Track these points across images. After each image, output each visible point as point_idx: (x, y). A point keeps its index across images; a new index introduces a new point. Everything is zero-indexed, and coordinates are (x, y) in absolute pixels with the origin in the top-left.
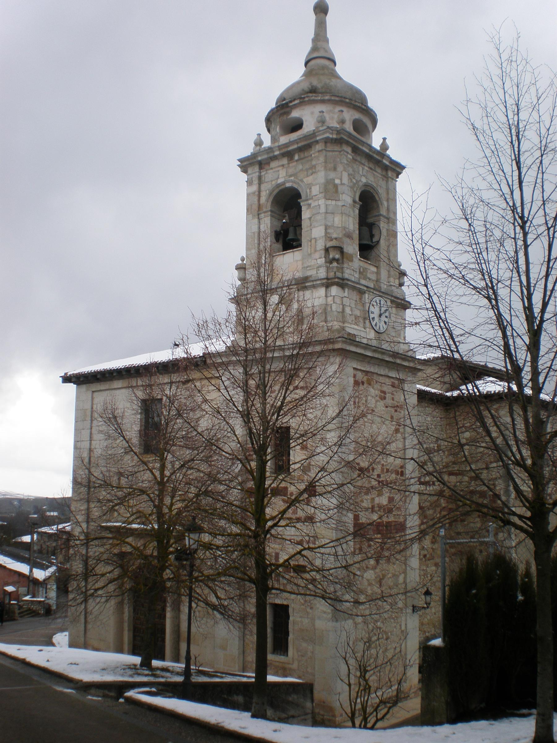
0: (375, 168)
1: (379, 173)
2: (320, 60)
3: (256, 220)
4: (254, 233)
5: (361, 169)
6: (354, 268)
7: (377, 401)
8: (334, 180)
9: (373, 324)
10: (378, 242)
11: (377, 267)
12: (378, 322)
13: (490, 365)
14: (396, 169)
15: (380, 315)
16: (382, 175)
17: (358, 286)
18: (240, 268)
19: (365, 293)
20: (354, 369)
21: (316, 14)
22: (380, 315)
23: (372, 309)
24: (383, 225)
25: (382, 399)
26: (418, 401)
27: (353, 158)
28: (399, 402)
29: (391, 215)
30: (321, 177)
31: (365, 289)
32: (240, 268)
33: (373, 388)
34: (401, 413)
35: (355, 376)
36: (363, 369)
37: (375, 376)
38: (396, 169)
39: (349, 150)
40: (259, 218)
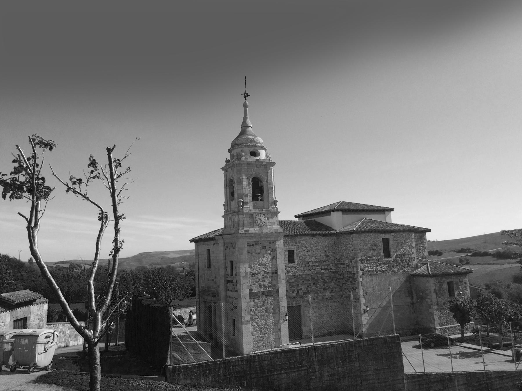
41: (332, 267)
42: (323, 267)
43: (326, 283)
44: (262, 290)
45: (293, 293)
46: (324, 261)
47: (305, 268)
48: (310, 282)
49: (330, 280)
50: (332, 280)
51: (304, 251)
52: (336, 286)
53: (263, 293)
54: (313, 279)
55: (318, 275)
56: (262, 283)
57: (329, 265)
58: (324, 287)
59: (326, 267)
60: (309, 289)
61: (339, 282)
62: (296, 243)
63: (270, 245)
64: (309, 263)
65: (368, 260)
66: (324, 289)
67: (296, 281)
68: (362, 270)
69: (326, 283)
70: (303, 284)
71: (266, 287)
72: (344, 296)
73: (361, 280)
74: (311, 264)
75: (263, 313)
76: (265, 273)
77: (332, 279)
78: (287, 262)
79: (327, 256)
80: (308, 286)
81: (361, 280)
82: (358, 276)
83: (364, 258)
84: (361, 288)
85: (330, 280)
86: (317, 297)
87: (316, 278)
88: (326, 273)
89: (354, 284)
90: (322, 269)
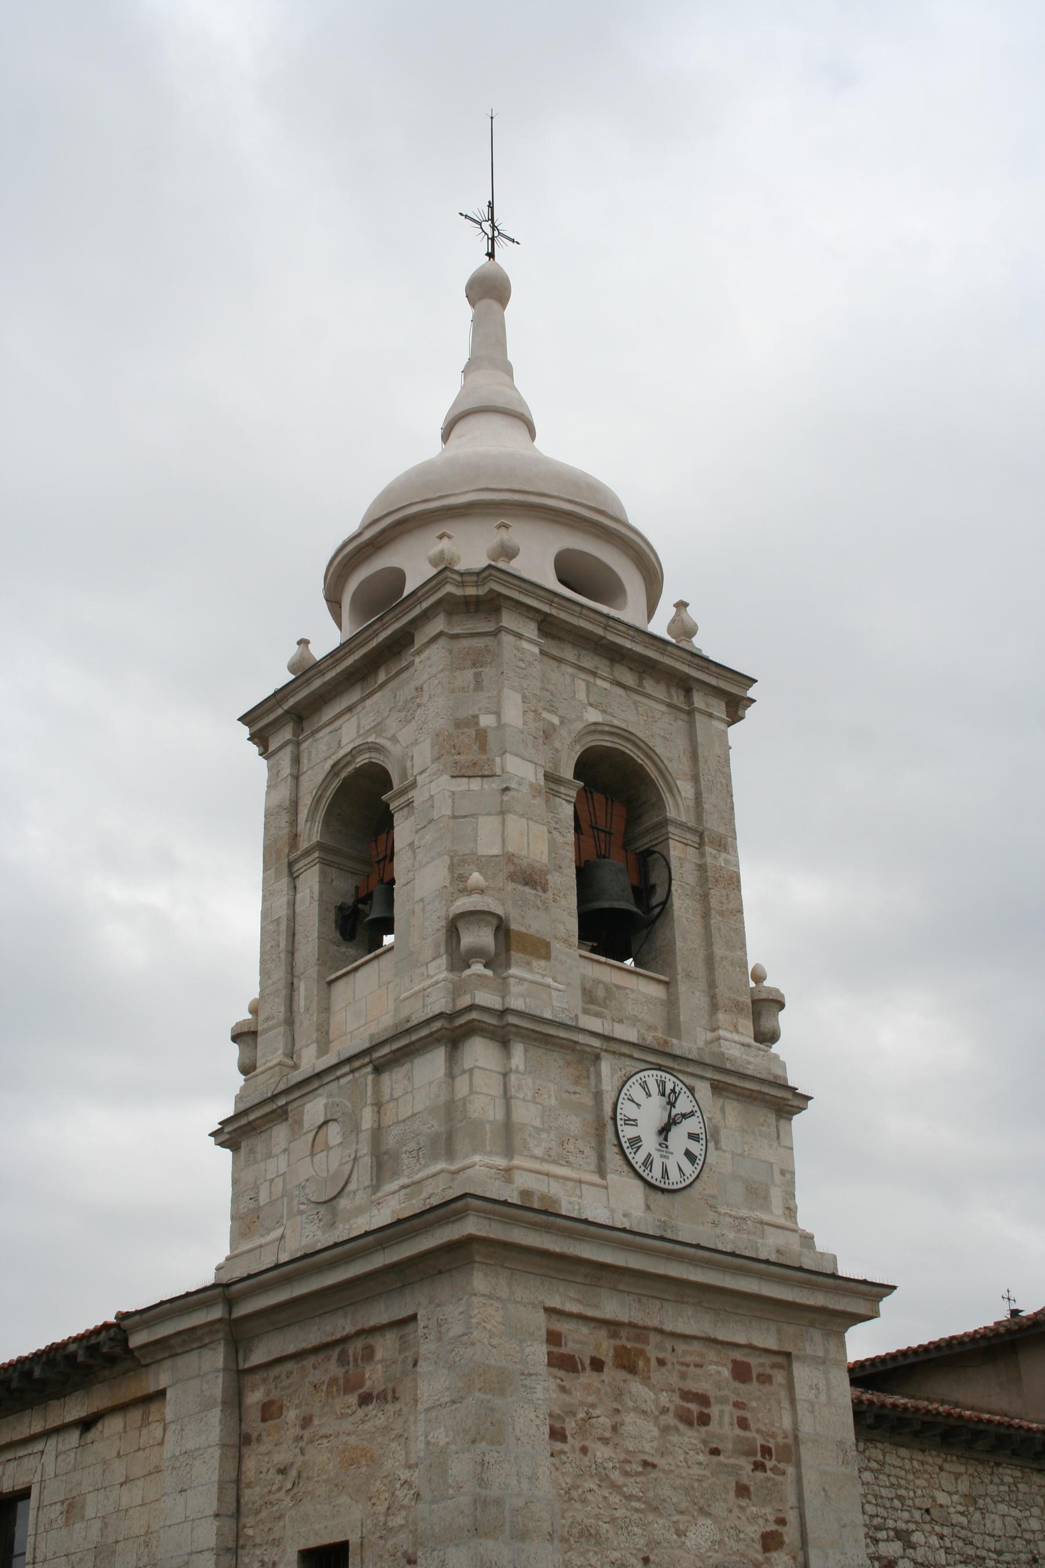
0: (640, 685)
3: (285, 881)
4: (278, 921)
5: (581, 686)
6: (559, 979)
7: (665, 1430)
8: (476, 717)
9: (638, 1159)
10: (666, 903)
11: (666, 983)
12: (656, 1155)
14: (733, 694)
15: (664, 1131)
16: (669, 705)
17: (581, 1038)
18: (243, 1036)
19: (597, 1058)
20: (550, 1311)
21: (473, 303)
22: (664, 1131)
23: (626, 1109)
24: (680, 855)
25: (690, 1424)
26: (858, 1434)
27: (542, 652)
28: (773, 1435)
29: (712, 823)
30: (436, 711)
31: (596, 1043)
32: (243, 1036)
33: (646, 1380)
34: (784, 1473)
35: (553, 1338)
36: (590, 1313)
37: (654, 1338)
38: (733, 694)
39: (530, 630)
40: (291, 873)
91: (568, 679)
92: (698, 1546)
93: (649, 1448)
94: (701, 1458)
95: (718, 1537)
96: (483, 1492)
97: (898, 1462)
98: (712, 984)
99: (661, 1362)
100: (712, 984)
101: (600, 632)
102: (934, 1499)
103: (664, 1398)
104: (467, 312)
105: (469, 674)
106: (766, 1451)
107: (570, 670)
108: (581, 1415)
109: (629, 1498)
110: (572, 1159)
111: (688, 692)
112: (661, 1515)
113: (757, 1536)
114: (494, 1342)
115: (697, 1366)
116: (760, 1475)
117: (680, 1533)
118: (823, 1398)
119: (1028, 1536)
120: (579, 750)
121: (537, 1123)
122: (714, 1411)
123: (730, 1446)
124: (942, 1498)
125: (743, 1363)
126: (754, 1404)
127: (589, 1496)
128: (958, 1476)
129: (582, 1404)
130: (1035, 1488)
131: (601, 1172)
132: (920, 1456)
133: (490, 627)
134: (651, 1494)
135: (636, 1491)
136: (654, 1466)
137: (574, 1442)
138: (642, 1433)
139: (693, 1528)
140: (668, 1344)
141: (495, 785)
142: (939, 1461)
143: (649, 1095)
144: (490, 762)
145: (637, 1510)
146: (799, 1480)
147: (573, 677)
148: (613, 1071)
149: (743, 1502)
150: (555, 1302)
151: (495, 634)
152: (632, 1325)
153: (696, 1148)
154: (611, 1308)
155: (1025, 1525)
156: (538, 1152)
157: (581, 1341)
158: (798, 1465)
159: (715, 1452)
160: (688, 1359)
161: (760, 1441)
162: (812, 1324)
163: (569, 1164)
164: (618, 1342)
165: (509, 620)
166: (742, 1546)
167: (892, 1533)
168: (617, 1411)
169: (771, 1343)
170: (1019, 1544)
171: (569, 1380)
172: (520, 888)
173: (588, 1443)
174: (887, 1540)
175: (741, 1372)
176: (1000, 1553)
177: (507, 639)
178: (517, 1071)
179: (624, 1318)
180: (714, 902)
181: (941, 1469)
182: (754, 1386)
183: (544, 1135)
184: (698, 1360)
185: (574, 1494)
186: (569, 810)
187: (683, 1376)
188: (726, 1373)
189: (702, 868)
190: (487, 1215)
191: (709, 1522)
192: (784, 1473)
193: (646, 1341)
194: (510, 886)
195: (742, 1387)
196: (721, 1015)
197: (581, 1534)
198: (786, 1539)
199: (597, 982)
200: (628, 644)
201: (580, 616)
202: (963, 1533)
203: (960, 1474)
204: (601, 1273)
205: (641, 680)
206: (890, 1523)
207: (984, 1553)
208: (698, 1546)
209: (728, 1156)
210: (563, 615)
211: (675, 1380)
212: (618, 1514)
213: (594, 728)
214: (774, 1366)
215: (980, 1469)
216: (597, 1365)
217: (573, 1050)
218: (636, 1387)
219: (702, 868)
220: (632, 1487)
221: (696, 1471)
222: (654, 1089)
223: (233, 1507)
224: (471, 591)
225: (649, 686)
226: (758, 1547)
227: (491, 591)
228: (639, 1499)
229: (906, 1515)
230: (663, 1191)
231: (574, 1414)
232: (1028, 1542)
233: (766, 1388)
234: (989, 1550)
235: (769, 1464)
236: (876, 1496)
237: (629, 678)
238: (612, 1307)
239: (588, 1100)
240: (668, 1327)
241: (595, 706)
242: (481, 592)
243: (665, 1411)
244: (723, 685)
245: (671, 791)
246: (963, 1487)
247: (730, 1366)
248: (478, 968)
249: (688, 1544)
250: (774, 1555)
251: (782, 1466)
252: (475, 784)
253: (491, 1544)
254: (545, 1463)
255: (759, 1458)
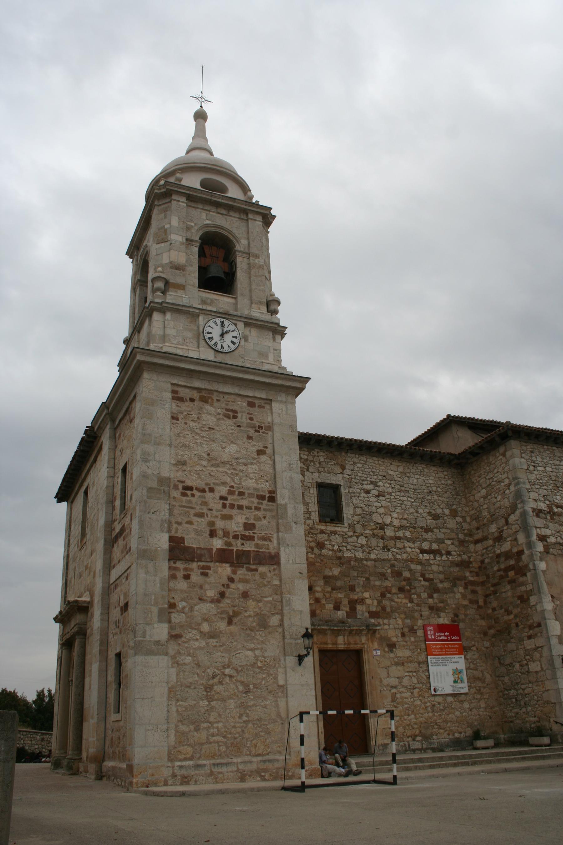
1: (213, 212)
2: (199, 142)
8: (164, 226)
13: (283, 395)
17: (191, 310)
19: (198, 316)
20: (172, 384)
22: (222, 335)
27: (187, 206)
28: (264, 423)
31: (197, 311)
33: (212, 405)
35: (174, 392)
36: (188, 385)
37: (215, 393)
39: (184, 199)
41: (451, 548)
42: (426, 546)
43: (437, 590)
44: (218, 543)
45: (337, 607)
46: (428, 530)
47: (374, 542)
48: (388, 584)
49: (446, 585)
50: (455, 585)
51: (368, 492)
52: (466, 602)
53: (224, 556)
54: (398, 574)
55: (413, 566)
56: (220, 524)
57: (440, 541)
58: (431, 601)
59: (435, 546)
60: (386, 602)
61: (474, 592)
62: (343, 468)
63: (251, 410)
64: (382, 527)
65: (554, 514)
66: (431, 608)
67: (344, 574)
68: (542, 538)
69: (437, 590)
70: (367, 586)
71: (236, 537)
72: (492, 632)
73: (542, 566)
74: (389, 532)
75: (222, 625)
76: (231, 492)
77: (455, 581)
78: (315, 516)
79: (436, 517)
80: (383, 595)
81: (542, 566)
82: (531, 556)
83: (543, 506)
84: (545, 588)
85: (446, 585)
86: (412, 631)
87: (406, 574)
88: (436, 565)
89: (523, 584)
90: (423, 551)
91: (199, 213)
92: (230, 452)
93: (211, 424)
94: (233, 428)
95: (238, 450)
96: (144, 432)
97: (373, 461)
98: (251, 297)
99: (218, 400)
100: (251, 297)
101: (210, 198)
102: (387, 473)
103: (219, 411)
104: (194, 123)
105: (163, 215)
106: (260, 427)
107: (200, 210)
108: (185, 413)
109: (203, 437)
110: (188, 344)
111: (247, 214)
112: (215, 443)
113: (255, 450)
114: (151, 391)
115: (232, 402)
116: (257, 434)
117: (223, 448)
118: (284, 412)
119: (427, 485)
120: (201, 233)
121: (175, 334)
122: (239, 415)
123: (245, 425)
124: (391, 472)
125: (252, 402)
126: (256, 414)
127: (187, 436)
128: (398, 466)
129: (185, 410)
130: (432, 471)
131: (198, 347)
132: (382, 460)
133: (168, 200)
134: (212, 436)
135: (205, 435)
136: (213, 429)
137: (181, 422)
138: (209, 419)
139: (228, 447)
140: (222, 396)
141: (168, 243)
142: (390, 462)
143: (217, 325)
144: (167, 237)
145: (206, 441)
146: (273, 436)
147: (201, 212)
148: (204, 319)
149: (250, 441)
150: (175, 381)
151: (170, 202)
152: (205, 389)
153: (235, 340)
154: (197, 384)
155: (426, 481)
156: (175, 342)
157: (183, 393)
158: (273, 432)
159: (239, 426)
160: (229, 400)
161: (257, 424)
162: (281, 391)
163: (186, 345)
164: (201, 394)
165: (174, 197)
166: (248, 453)
167: (369, 482)
168: (200, 413)
169: (263, 396)
170: (424, 487)
171: (180, 404)
172: (174, 270)
173: (188, 422)
174: (367, 484)
175: (251, 405)
176: (415, 489)
177: (173, 202)
178: (168, 320)
179: (203, 387)
180: (252, 273)
181: (391, 464)
182: (257, 409)
183: (177, 338)
184: (233, 400)
185: (180, 435)
186: (196, 249)
187: (227, 405)
188: (245, 404)
189: (249, 264)
190: (143, 354)
191: (235, 445)
192: (267, 434)
193: (213, 394)
194: (171, 270)
195: (251, 409)
196: (253, 305)
197: (183, 446)
198: (267, 452)
199: (207, 298)
200: (220, 201)
201: (201, 193)
202: (399, 483)
203: (399, 466)
204: (191, 373)
205: (228, 213)
206: (368, 479)
207: (408, 489)
208: (230, 452)
209: (252, 344)
210: (194, 194)
211: (223, 405)
212: (198, 441)
213: (207, 226)
214: (265, 403)
215: (408, 464)
216: (192, 400)
217: (189, 314)
218: (208, 407)
219: (249, 264)
220: (204, 434)
221: (231, 431)
222: (219, 323)
223: (113, 466)
224: (162, 190)
225: (232, 213)
226: (255, 454)
227: (167, 189)
228: (207, 438)
229: (375, 477)
230: (222, 352)
231: (182, 413)
232: (428, 487)
233: (262, 409)
234: (411, 489)
235: (261, 431)
236: (363, 471)
237: (223, 212)
238: (197, 384)
239: (196, 328)
240: (220, 390)
241: (205, 219)
242: (165, 190)
243: (219, 414)
244: (259, 210)
245: (238, 242)
246: (401, 469)
247: (247, 402)
248: (159, 293)
249: (226, 451)
250: (262, 456)
251: (267, 432)
252: (163, 245)
253: (146, 445)
254: (168, 426)
255: (257, 429)
